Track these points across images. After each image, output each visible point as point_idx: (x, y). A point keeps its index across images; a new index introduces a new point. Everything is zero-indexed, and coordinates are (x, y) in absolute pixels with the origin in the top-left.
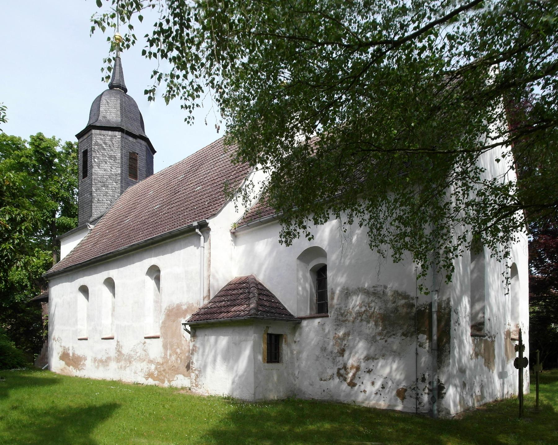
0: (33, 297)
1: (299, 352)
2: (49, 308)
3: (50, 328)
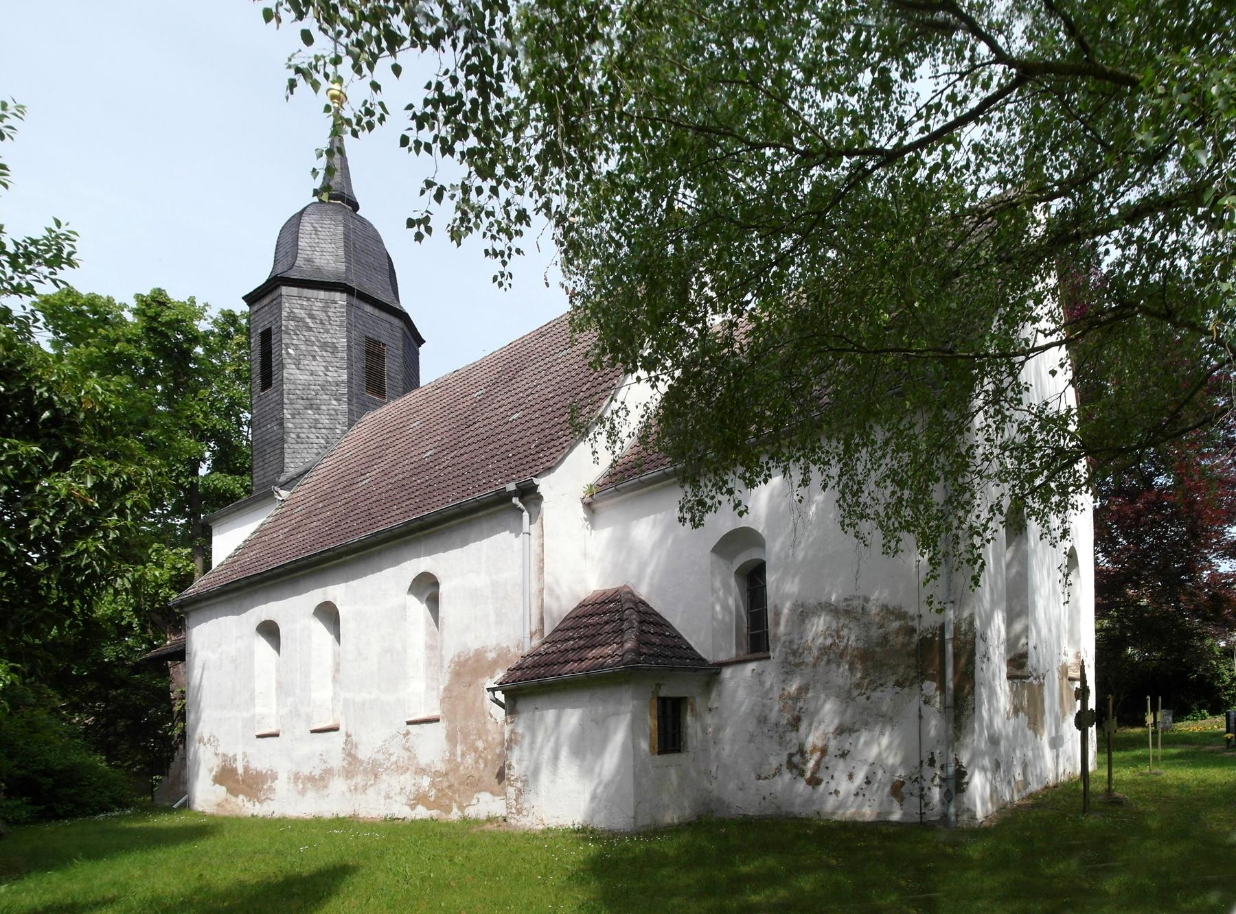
0: (148, 650)
1: (718, 729)
2: (187, 673)
3: (191, 717)
